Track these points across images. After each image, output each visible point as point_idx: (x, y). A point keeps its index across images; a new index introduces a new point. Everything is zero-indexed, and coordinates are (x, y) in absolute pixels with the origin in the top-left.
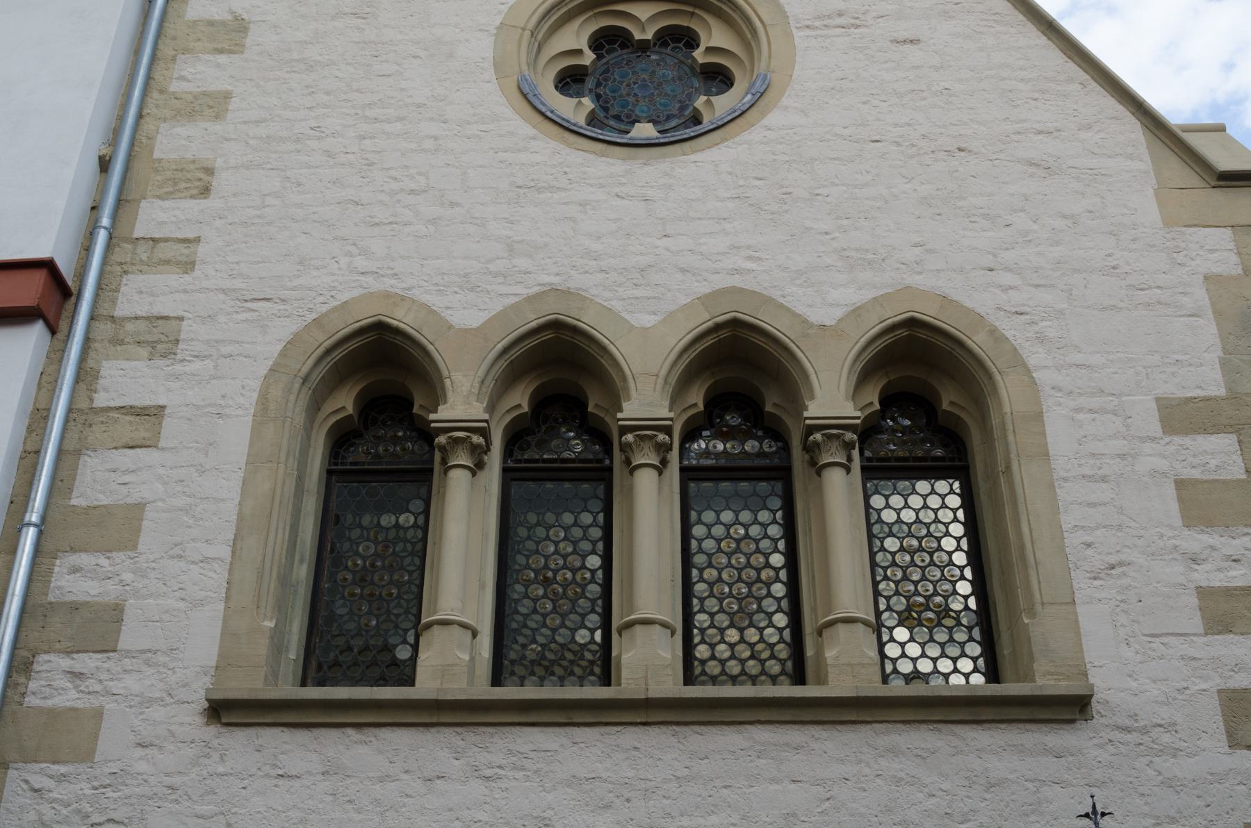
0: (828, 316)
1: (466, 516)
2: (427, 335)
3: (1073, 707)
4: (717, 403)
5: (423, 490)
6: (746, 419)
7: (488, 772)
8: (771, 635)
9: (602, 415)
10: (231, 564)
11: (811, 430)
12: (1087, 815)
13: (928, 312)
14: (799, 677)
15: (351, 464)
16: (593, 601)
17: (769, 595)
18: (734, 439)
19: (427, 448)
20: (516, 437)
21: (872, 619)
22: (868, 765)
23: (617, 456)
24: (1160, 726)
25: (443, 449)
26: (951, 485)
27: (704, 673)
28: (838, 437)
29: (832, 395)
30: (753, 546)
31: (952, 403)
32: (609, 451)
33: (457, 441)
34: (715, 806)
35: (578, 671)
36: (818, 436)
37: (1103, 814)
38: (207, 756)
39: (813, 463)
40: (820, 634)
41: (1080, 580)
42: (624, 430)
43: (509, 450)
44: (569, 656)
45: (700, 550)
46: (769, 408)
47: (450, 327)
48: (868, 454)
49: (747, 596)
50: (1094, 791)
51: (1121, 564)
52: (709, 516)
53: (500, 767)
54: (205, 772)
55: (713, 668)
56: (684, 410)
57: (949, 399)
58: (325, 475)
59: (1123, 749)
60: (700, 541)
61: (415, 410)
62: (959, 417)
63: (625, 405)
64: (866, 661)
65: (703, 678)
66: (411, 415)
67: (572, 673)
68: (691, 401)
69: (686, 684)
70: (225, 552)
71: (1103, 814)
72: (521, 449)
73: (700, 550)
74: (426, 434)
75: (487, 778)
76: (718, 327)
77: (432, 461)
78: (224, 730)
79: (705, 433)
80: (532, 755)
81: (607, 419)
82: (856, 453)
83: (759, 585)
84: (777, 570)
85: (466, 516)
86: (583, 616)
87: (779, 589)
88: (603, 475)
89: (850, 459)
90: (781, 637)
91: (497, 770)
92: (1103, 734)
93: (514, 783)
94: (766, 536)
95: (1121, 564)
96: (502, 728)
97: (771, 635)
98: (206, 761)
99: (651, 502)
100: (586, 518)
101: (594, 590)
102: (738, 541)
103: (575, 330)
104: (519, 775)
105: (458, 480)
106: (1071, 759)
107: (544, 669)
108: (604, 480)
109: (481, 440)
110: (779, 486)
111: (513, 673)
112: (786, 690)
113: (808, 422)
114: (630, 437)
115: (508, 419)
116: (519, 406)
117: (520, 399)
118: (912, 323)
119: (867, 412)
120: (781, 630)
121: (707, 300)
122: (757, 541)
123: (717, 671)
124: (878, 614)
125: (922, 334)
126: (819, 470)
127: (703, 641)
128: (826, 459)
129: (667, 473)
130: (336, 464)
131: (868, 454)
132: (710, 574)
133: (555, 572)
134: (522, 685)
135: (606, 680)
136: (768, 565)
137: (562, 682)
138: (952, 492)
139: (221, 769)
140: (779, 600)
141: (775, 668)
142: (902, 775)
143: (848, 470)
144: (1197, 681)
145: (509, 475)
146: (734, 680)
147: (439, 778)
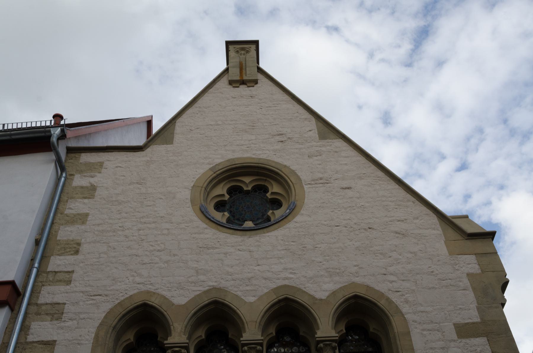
0: (322, 295)
11: (319, 342)
28: (329, 345)
36: (321, 345)
57: (372, 328)
121: (275, 290)
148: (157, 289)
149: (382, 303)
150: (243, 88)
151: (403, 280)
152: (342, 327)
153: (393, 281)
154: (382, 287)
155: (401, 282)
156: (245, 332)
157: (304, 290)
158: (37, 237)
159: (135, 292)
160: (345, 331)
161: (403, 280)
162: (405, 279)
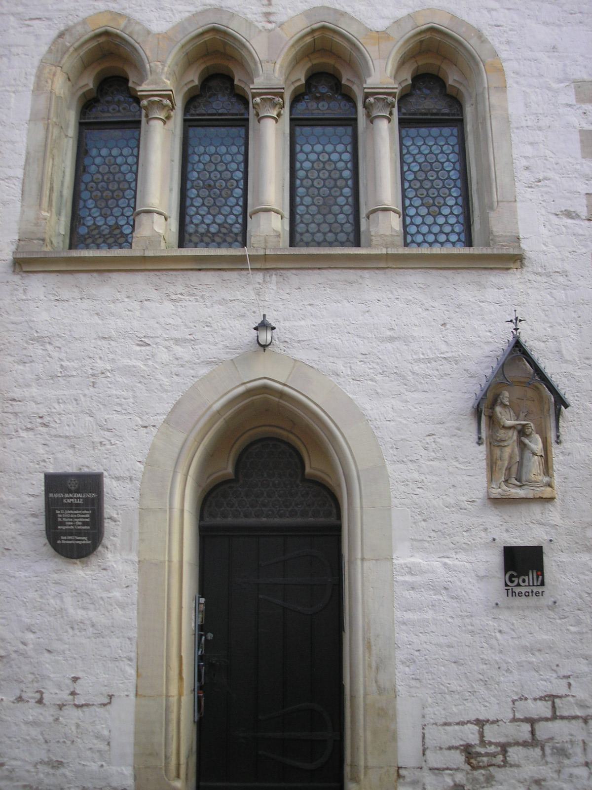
0: (379, 25)
1: (161, 147)
2: (136, 38)
3: (512, 260)
4: (315, 77)
5: (136, 134)
6: (331, 88)
7: (174, 297)
8: (341, 218)
9: (243, 86)
10: (24, 180)
11: (367, 95)
12: (511, 321)
13: (441, 22)
14: (469, 243)
15: (94, 118)
16: (237, 199)
17: (341, 195)
18: (323, 100)
19: (138, 108)
20: (191, 101)
21: (400, 209)
22: (392, 292)
23: (252, 111)
24: (558, 272)
25: (146, 108)
26: (452, 131)
27: (302, 240)
28: (383, 99)
29: (382, 72)
30: (333, 166)
31: (348, 80)
32: (247, 108)
33: (153, 102)
34: (304, 315)
35: (229, 239)
36: (372, 99)
37: (520, 321)
38: (16, 290)
39: (368, 115)
40: (368, 217)
41: (520, 188)
42: (254, 96)
43: (187, 108)
44: (95, 232)
45: (301, 168)
46: (344, 82)
47: (149, 32)
48: (403, 111)
49: (329, 196)
50: (518, 308)
51: (545, 179)
52: (307, 148)
53: (181, 294)
54: (15, 299)
55: (307, 237)
56: (186, 84)
57: (452, 79)
58: (78, 125)
59: (535, 285)
60: (301, 163)
61: (131, 84)
62: (458, 90)
63: (256, 80)
64: (394, 233)
65: (302, 243)
66: (128, 88)
67: (225, 241)
68: (191, 78)
69: (290, 246)
70: (20, 173)
71: (520, 321)
72: (195, 107)
73: (301, 168)
74: (137, 100)
75: (173, 300)
76: (313, 31)
77: (140, 116)
78: (24, 275)
79: (306, 97)
80: (200, 287)
81: (246, 89)
82: (395, 111)
83: (335, 189)
84: (346, 180)
85: (161, 147)
86: (231, 207)
87: (347, 191)
88: (243, 123)
89: (391, 114)
90: (348, 220)
91: (180, 296)
92: (525, 276)
93: (190, 303)
94: (341, 160)
95: (545, 179)
96: (344, 270)
97: (341, 218)
98: (15, 293)
99: (271, 138)
100: (234, 149)
101: (238, 192)
102: (324, 163)
103: (225, 33)
104: (192, 298)
105: (157, 125)
106: (506, 290)
107: (208, 239)
108: (351, 125)
109: (169, 102)
110: (455, 131)
111: (190, 241)
112: (466, 251)
113: (366, 90)
114: (258, 100)
115: (186, 89)
116: (193, 81)
117: (194, 78)
118: (432, 30)
119: (404, 85)
120: (347, 215)
121: (307, 14)
122: (335, 163)
123: (310, 239)
124: (404, 208)
125: (330, 35)
126: (371, 119)
127: (302, 222)
128: (375, 113)
129: (280, 121)
130: (84, 119)
131: (403, 111)
132: (307, 183)
133: (215, 181)
134: (196, 247)
135: (244, 244)
136: (341, 177)
137: (219, 246)
138: (452, 135)
139: (24, 297)
140: (347, 198)
141: (454, 238)
142: (411, 298)
143: (389, 120)
144: (581, 247)
145: (188, 123)
146: (319, 244)
147: (146, 300)
148: (124, 9)
149: (472, 44)
150: (499, 24)
151: (509, 9)
152: (407, 77)
153: (493, 10)
154: (474, 18)
155: (506, 11)
156: (259, 76)
157: (353, 14)
158: (166, 116)
159: (91, 12)
160: (410, 82)
161: (509, 9)
162: (511, 7)
